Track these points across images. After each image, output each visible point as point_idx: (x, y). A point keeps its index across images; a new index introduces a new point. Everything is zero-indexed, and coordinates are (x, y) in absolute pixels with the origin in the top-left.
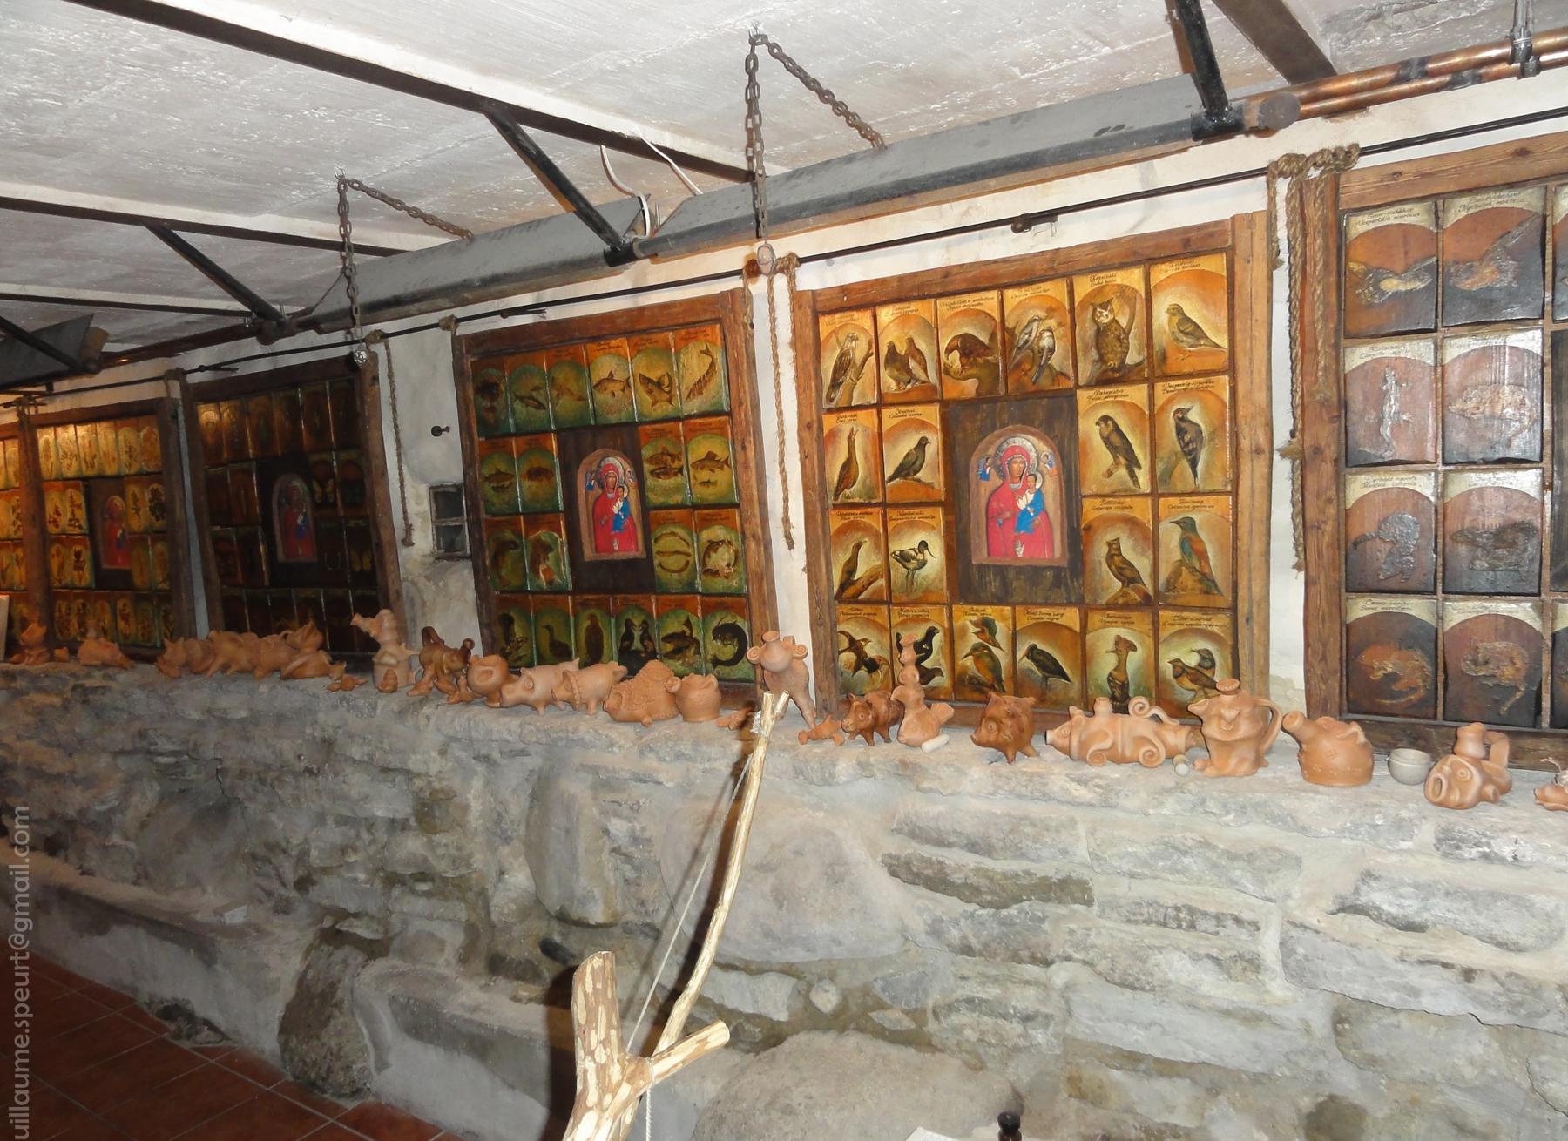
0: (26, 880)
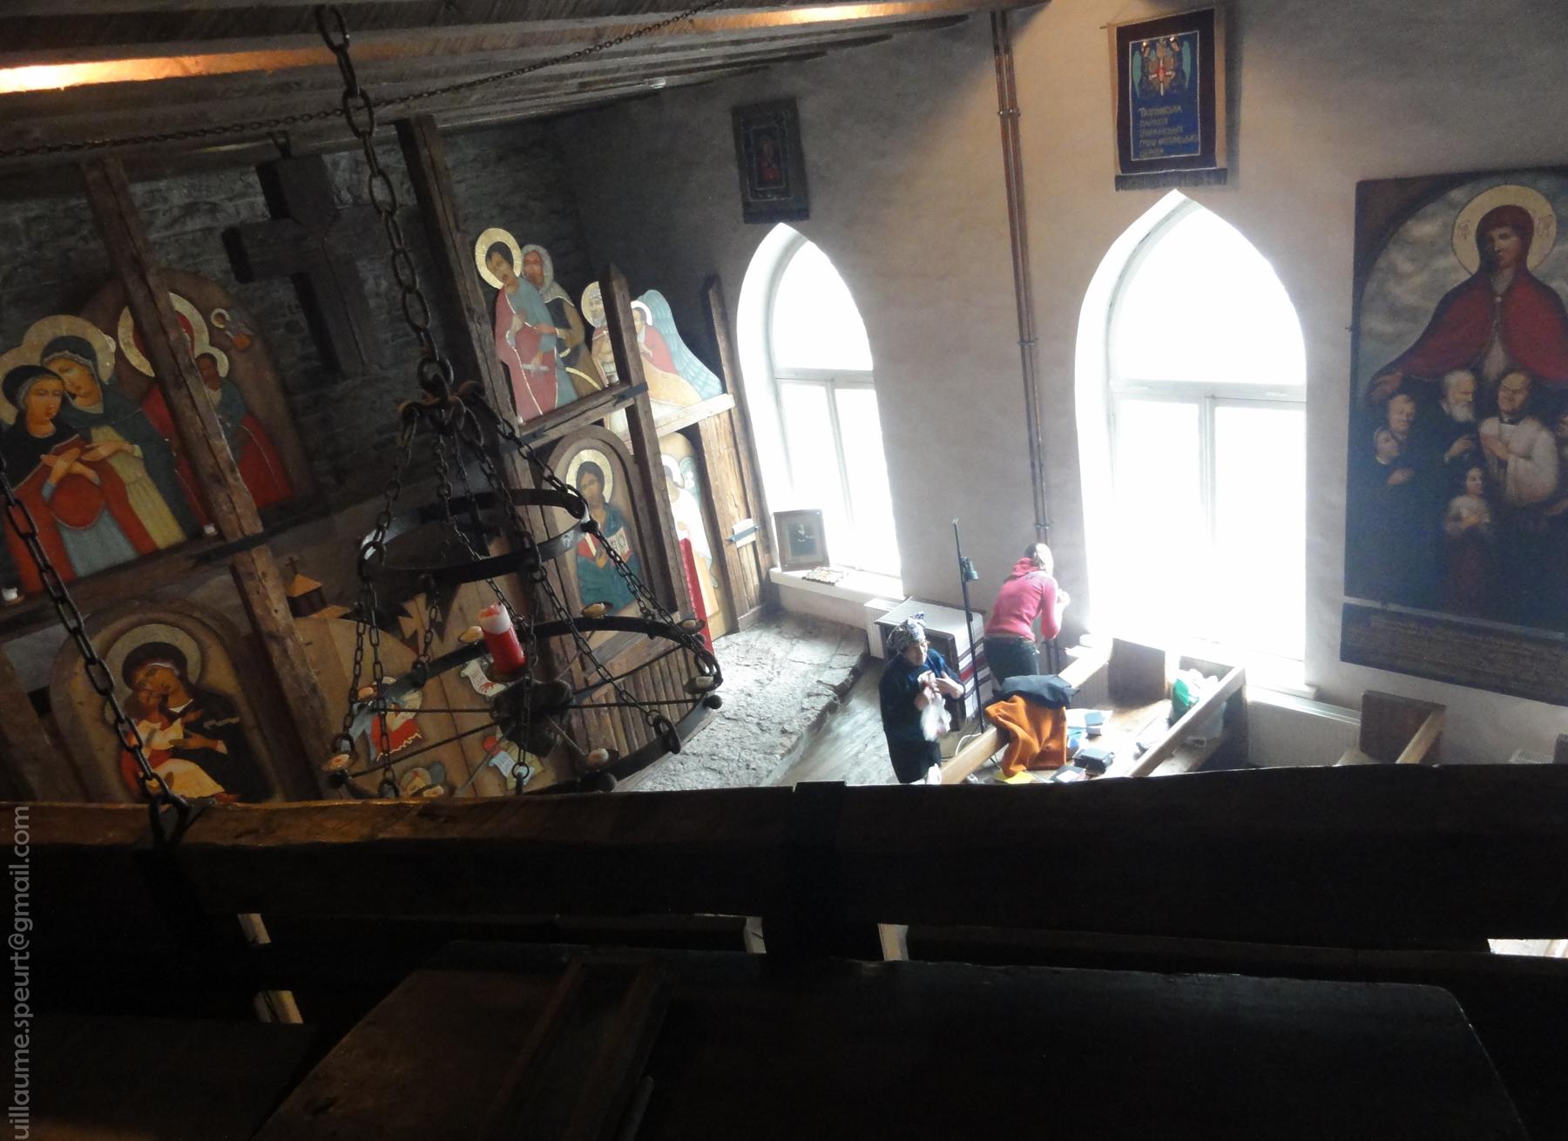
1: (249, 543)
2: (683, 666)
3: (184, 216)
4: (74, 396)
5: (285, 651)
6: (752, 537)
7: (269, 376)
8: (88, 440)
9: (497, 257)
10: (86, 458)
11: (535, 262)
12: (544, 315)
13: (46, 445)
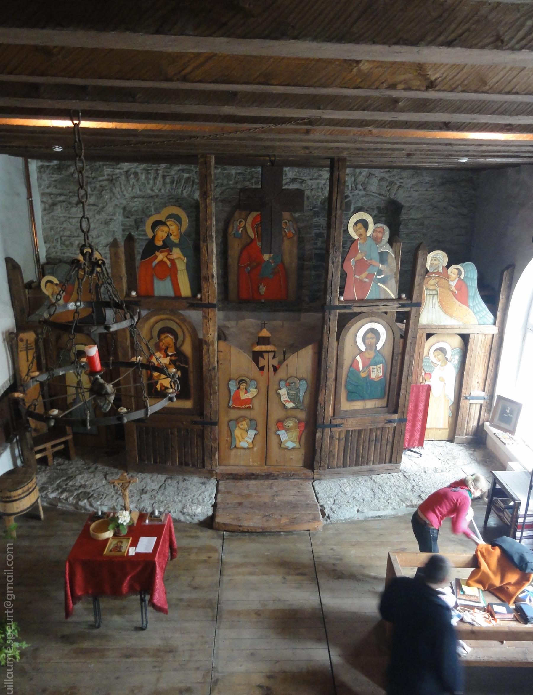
0: (12, 576)
1: (213, 306)
2: (391, 440)
3: (290, 182)
4: (171, 235)
5: (208, 350)
6: (482, 402)
7: (295, 251)
8: (171, 251)
9: (360, 225)
10: (169, 257)
12: (376, 256)
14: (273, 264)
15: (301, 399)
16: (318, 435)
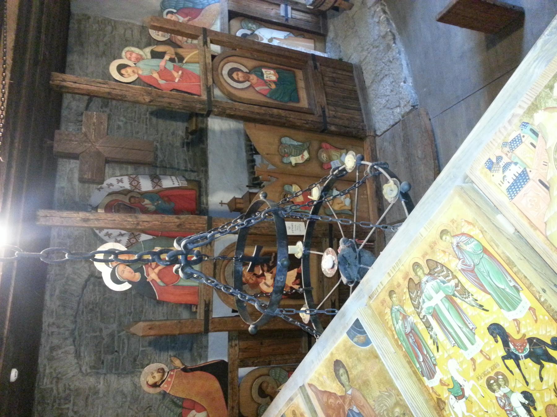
6: (289, 8)
9: (123, 71)
11: (131, 55)
12: (156, 62)
13: (143, 278)
14: (160, 202)
15: (300, 143)
16: (333, 128)
